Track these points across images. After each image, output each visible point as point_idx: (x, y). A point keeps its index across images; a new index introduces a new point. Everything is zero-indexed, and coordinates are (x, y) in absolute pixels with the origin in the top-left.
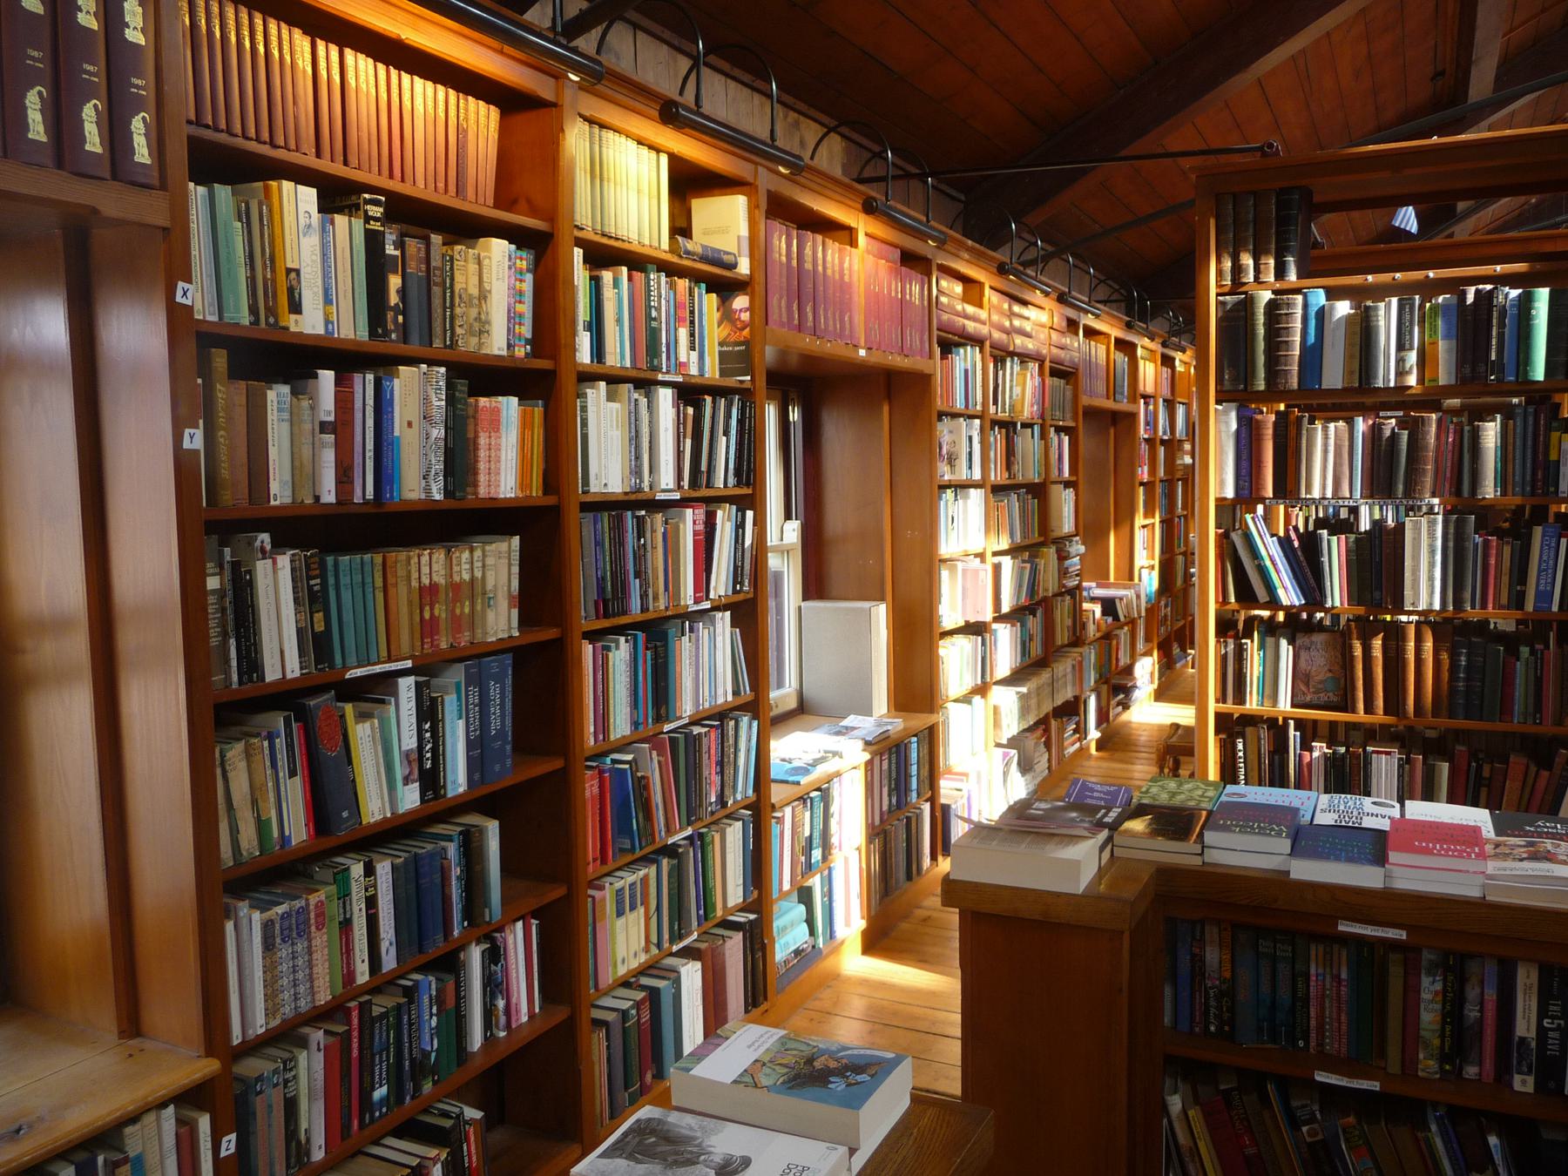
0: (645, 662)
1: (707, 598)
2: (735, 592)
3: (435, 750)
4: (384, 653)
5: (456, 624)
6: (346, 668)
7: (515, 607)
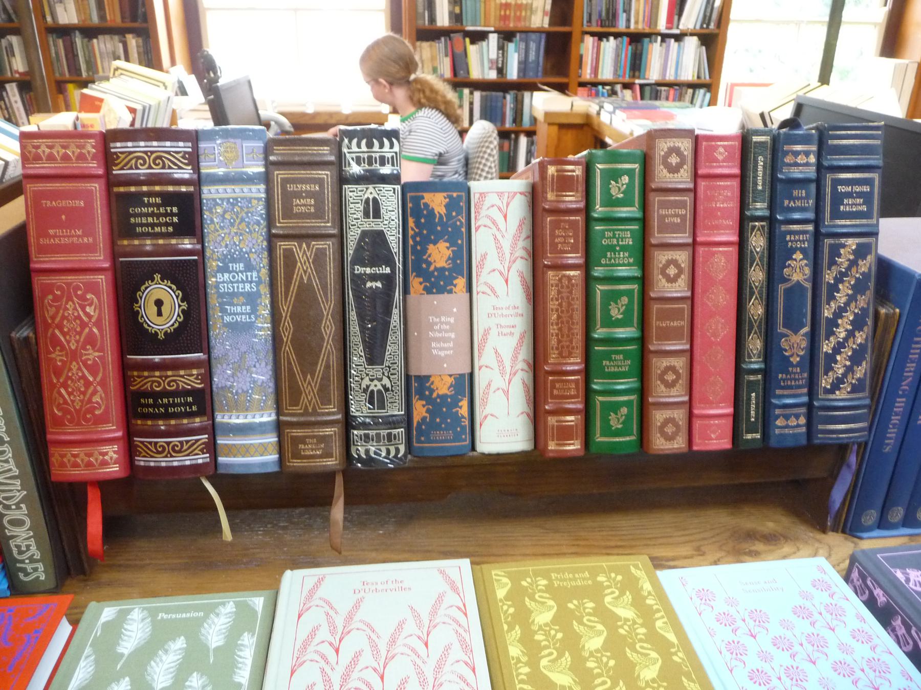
0: (316, 223)
1: (678, 28)
2: (702, 27)
3: (503, 61)
4: (483, 23)
5: (519, 19)
6: (467, 26)
7: (547, 15)
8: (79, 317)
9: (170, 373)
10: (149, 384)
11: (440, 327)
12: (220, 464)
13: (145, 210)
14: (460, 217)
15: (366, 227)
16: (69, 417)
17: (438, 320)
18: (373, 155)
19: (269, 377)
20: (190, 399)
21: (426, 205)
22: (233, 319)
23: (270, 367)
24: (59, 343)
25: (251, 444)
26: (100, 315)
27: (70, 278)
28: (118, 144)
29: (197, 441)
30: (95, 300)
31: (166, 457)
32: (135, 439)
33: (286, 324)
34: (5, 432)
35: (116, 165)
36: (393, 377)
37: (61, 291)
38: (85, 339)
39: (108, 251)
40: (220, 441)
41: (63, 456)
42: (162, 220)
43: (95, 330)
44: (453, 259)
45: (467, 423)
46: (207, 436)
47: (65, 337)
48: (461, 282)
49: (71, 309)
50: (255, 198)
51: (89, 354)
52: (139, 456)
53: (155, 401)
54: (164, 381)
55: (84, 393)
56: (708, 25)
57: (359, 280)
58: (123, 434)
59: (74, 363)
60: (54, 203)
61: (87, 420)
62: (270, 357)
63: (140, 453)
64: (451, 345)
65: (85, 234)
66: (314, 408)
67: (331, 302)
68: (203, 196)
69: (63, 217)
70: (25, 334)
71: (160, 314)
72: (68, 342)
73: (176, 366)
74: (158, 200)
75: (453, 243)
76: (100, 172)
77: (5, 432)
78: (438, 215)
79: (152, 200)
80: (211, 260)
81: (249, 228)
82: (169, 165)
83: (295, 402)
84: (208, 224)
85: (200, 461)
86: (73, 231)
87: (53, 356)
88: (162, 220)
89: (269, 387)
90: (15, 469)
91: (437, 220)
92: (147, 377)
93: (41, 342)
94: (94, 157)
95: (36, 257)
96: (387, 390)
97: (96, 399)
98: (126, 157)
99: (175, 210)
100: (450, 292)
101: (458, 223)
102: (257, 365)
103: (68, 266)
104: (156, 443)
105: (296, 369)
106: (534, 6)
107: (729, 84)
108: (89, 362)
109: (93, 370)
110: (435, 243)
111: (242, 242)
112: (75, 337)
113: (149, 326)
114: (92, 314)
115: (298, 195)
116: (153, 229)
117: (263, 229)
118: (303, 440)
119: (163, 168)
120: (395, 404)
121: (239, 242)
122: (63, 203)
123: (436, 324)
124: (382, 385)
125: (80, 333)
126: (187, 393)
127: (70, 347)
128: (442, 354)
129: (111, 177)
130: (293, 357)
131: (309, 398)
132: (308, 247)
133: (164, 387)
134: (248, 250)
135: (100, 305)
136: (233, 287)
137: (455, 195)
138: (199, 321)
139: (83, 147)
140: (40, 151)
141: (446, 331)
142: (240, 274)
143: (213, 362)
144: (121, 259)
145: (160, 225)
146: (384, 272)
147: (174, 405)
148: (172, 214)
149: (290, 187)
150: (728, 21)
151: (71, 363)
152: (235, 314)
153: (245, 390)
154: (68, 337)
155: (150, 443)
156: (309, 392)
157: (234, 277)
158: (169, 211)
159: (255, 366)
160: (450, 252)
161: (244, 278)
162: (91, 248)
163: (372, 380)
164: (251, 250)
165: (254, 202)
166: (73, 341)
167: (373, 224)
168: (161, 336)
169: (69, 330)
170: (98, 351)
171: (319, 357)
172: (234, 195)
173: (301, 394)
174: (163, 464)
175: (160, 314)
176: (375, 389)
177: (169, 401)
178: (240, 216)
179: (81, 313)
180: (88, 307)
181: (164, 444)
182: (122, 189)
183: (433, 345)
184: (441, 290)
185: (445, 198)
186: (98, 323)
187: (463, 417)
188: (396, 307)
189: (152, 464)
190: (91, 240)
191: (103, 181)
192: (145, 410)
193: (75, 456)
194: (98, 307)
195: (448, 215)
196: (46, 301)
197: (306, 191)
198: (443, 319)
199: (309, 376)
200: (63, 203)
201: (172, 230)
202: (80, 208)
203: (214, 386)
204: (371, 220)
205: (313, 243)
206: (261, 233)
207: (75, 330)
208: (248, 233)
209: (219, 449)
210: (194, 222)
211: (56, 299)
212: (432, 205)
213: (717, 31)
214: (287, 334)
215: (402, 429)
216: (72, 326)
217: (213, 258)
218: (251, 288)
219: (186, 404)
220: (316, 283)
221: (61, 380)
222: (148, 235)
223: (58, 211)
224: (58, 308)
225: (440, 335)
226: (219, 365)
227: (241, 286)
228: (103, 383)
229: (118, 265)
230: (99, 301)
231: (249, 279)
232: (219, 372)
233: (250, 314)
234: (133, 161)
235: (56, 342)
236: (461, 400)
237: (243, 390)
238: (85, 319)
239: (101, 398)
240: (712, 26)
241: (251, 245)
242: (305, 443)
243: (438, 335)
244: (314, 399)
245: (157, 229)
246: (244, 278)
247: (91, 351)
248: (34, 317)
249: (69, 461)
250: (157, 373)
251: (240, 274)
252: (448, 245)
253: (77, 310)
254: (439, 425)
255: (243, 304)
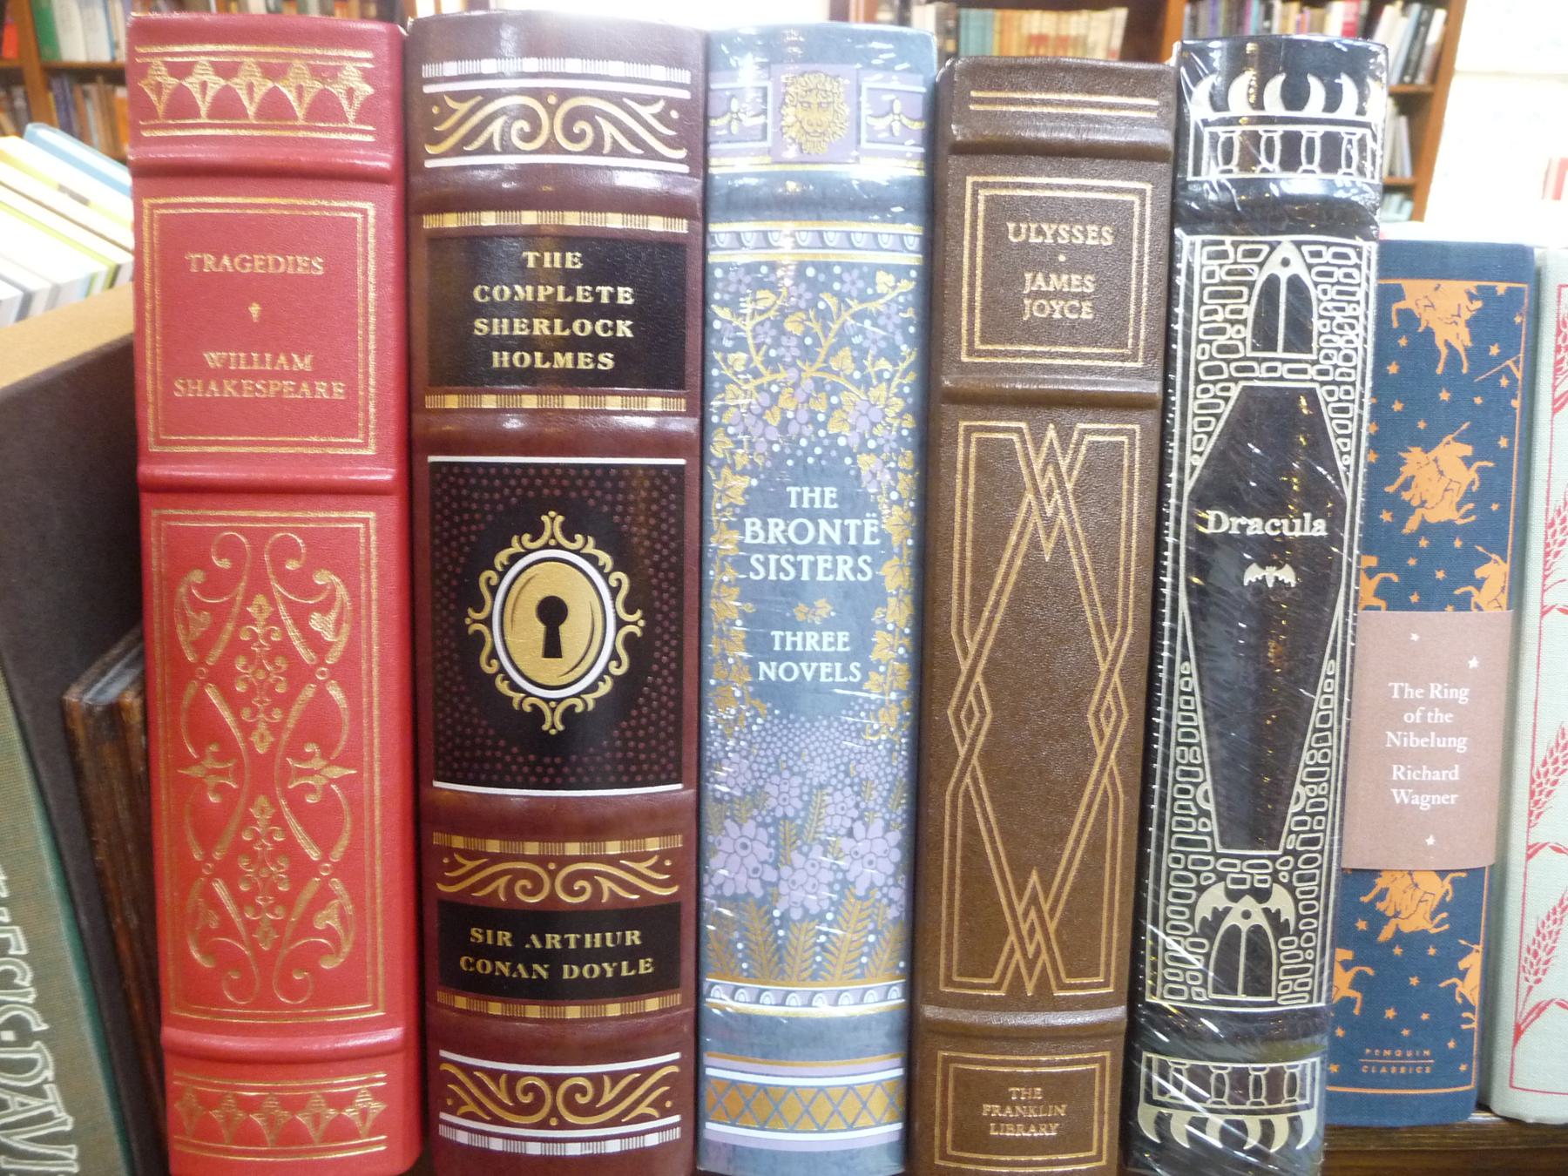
2: (1401, 81)
8: (284, 648)
9: (573, 849)
10: (502, 882)
11: (1424, 717)
12: (708, 1142)
13: (524, 293)
14: (1509, 363)
15: (1261, 378)
16: (235, 976)
17: (1418, 693)
18: (1304, 130)
19: (890, 869)
20: (633, 937)
21: (1408, 317)
22: (789, 672)
23: (895, 836)
24: (215, 731)
25: (821, 1089)
26: (353, 643)
27: (266, 514)
28: (450, 68)
29: (647, 1072)
30: (342, 592)
31: (543, 1125)
32: (444, 1054)
33: (971, 697)
34: (35, 1006)
35: (438, 139)
36: (1305, 886)
37: (232, 559)
38: (300, 722)
39: (392, 430)
40: (718, 1069)
41: (209, 1102)
42: (583, 327)
43: (336, 693)
44: (1477, 497)
45: (1474, 1025)
46: (676, 1056)
47: (236, 714)
48: (1495, 572)
49: (262, 727)
50: (887, 268)
51: (311, 773)
52: (452, 1112)
53: (520, 938)
54: (553, 875)
55: (287, 901)
56: (1414, 76)
57: (1204, 552)
58: (406, 1034)
59: (262, 801)
60: (226, 261)
61: (293, 991)
62: (899, 811)
63: (460, 1102)
64: (1454, 775)
65: (320, 372)
66: (1043, 984)
67: (1124, 628)
68: (713, 258)
69: (255, 309)
70: (112, 693)
71: (553, 648)
72: (247, 729)
73: (594, 827)
74: (573, 260)
75: (1482, 443)
76: (384, 161)
77: (35, 1006)
78: (1444, 352)
79: (553, 260)
80: (725, 471)
81: (862, 368)
82: (615, 142)
83: (981, 956)
84: (726, 351)
85: (652, 1140)
86: (282, 359)
87: (195, 771)
88: (583, 327)
89: (891, 902)
90: (62, 1115)
91: (1439, 370)
92: (496, 859)
93: (160, 719)
94: (365, 113)
95: (160, 443)
96: (1280, 928)
97: (327, 919)
98: (472, 111)
99: (625, 296)
100: (1463, 604)
101: (1504, 382)
102: (859, 828)
103: (261, 475)
104: (514, 1077)
105: (995, 852)
106: (1091, 39)
107: (1556, 161)
108: (311, 799)
109: (322, 823)
110: (1428, 442)
111: (837, 414)
112: (268, 712)
113: (515, 687)
114: (329, 637)
115: (1044, 260)
116: (548, 358)
117: (904, 375)
118: (997, 1089)
119: (596, 149)
120: (1301, 978)
121: (829, 416)
122: (258, 263)
123: (1412, 705)
124: (1266, 911)
125: (285, 702)
126: (623, 916)
127: (251, 747)
128: (1423, 802)
129: (416, 180)
130: (987, 814)
131: (1031, 949)
132: (1064, 436)
133: (553, 895)
134: (855, 443)
135: (356, 610)
136: (798, 566)
137: (1501, 288)
138: (678, 674)
139: (334, 73)
140: (191, 83)
141: (1442, 731)
142: (823, 523)
143: (710, 809)
144: (432, 459)
145: (573, 344)
146: (1307, 533)
147: (583, 956)
148: (615, 311)
149: (1017, 233)
150: (1450, 73)
151: (251, 801)
152: (796, 657)
153: (814, 910)
154: (246, 714)
155: (495, 1075)
156: (1032, 931)
157: (801, 532)
158: (605, 300)
159: (850, 833)
160: (1472, 475)
161: (836, 537)
162: (339, 418)
163: (1234, 896)
164: (864, 442)
165: (884, 280)
166: (262, 727)
167: (1283, 369)
168: (553, 723)
169: (252, 690)
170: (341, 762)
171: (1072, 814)
172: (821, 255)
173: (1006, 934)
174: (534, 1149)
175: (553, 648)
176: (1245, 926)
177: (565, 942)
178: (835, 327)
179: (293, 633)
180: (316, 616)
181: (539, 1083)
182: (451, 221)
183: (1398, 773)
184: (1436, 598)
185: (1472, 297)
186: (347, 672)
187: (1467, 1006)
188: (1333, 656)
189: (497, 1145)
190: (339, 390)
191: (389, 193)
192: (484, 966)
193: (249, 1105)
194: (348, 615)
195: (1477, 353)
196: (183, 590)
197: (1070, 248)
198: (1435, 691)
199: (1034, 878)
200: (258, 263)
201: (611, 364)
202: (307, 279)
203: (709, 891)
204: (1280, 354)
205: (1081, 426)
206: (900, 386)
207: (271, 691)
208: (858, 384)
209: (709, 1096)
210: (682, 339)
211: (217, 583)
212: (1428, 318)
213: (1429, 89)
214: (969, 733)
215: (1317, 1060)
216: (261, 675)
217: (732, 467)
218: (856, 570)
219: (622, 953)
220: (1080, 563)
221: (217, 856)
222: (530, 379)
223: (239, 288)
224: (220, 615)
225: (1422, 742)
226: (728, 823)
227: (823, 562)
228: (351, 869)
229: (423, 480)
230: (354, 596)
231: (853, 541)
232: (727, 845)
233: (846, 659)
234: (496, 128)
235: (206, 729)
236: (1466, 951)
237: (806, 911)
238: (307, 655)
239: (343, 917)
240: (1421, 79)
241: (864, 425)
242: (1004, 1101)
243: (1414, 741)
244: (1044, 956)
245: (563, 360)
246: (836, 537)
247: (317, 763)
248: (141, 638)
249: (229, 1119)
250: (532, 848)
251: (823, 523)
252: (1468, 450)
253: (279, 622)
254: (1392, 1029)
255: (828, 625)
